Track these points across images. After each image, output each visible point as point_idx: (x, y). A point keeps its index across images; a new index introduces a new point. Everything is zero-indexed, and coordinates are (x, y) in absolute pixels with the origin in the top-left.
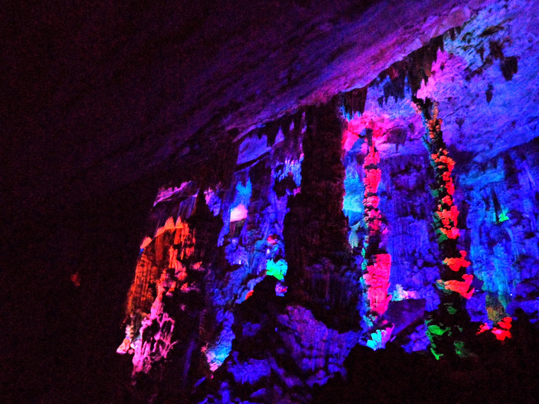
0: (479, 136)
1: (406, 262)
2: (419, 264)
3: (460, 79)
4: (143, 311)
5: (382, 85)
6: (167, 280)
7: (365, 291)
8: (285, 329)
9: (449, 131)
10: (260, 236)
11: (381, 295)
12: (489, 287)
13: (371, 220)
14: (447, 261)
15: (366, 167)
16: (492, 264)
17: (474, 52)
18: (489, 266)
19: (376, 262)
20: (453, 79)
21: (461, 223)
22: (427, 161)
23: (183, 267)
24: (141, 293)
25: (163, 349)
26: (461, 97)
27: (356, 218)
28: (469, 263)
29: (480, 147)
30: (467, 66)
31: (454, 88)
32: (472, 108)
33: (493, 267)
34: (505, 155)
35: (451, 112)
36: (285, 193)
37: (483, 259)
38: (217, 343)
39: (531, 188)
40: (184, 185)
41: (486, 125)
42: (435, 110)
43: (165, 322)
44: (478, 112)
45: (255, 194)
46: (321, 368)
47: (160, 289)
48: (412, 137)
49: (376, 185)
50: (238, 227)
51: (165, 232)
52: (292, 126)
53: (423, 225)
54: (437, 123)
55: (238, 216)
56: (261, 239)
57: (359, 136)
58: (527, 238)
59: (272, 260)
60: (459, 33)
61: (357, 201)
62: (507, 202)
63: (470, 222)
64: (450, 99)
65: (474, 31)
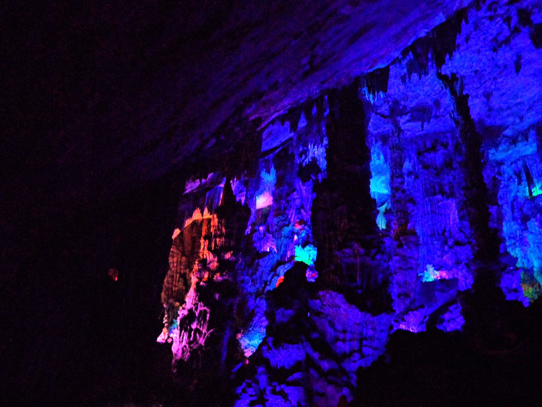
1: (436, 242)
4: (177, 300)
5: (404, 63)
6: (200, 271)
7: (395, 273)
8: (318, 314)
10: (287, 223)
17: (501, 22)
18: (523, 242)
23: (214, 257)
24: (172, 284)
25: (200, 337)
26: (487, 69)
29: (511, 120)
31: (480, 60)
33: (527, 242)
35: (479, 85)
36: (310, 177)
37: (516, 236)
38: (251, 329)
40: (210, 176)
43: (201, 311)
44: (506, 84)
45: (279, 181)
46: (354, 351)
47: (194, 280)
50: (264, 214)
51: (193, 222)
52: (314, 110)
55: (264, 203)
56: (288, 225)
59: (300, 246)
61: (383, 182)
63: (501, 198)
64: (476, 72)
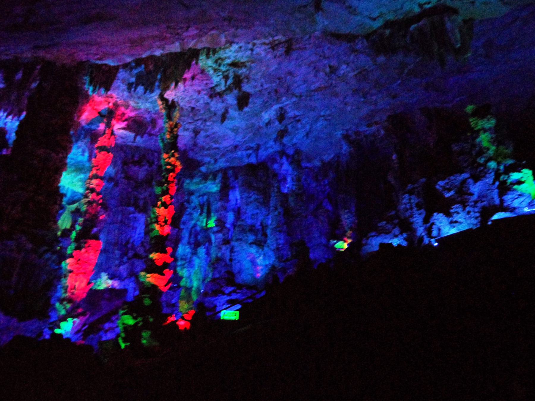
0: (209, 149)
2: (127, 255)
3: (205, 94)
5: (135, 72)
7: (65, 276)
9: (185, 136)
11: (82, 282)
12: (186, 282)
13: (89, 203)
14: (153, 256)
15: (97, 148)
16: (193, 263)
17: (221, 77)
18: (190, 264)
19: (84, 247)
20: (199, 92)
21: (176, 222)
22: (159, 159)
27: (76, 198)
28: (173, 259)
29: (207, 159)
30: (213, 85)
32: (208, 123)
34: (224, 171)
39: (236, 204)
41: (216, 142)
42: (176, 114)
44: (212, 128)
48: (152, 132)
49: (104, 168)
52: (19, 76)
53: (142, 218)
54: (176, 126)
57: (99, 113)
58: (223, 244)
60: (214, 54)
61: (81, 180)
62: (217, 211)
64: (193, 108)
65: (226, 58)
